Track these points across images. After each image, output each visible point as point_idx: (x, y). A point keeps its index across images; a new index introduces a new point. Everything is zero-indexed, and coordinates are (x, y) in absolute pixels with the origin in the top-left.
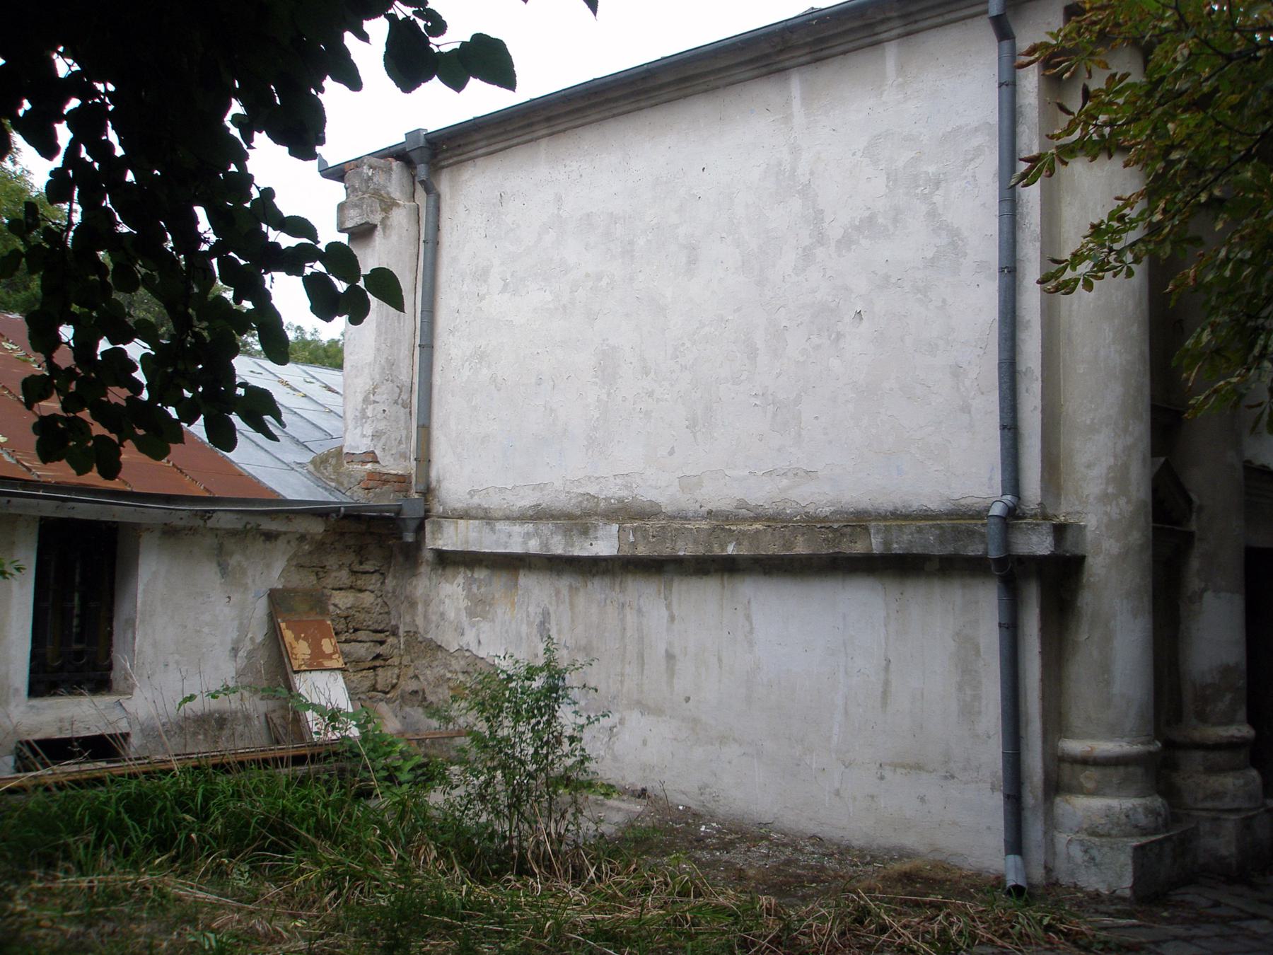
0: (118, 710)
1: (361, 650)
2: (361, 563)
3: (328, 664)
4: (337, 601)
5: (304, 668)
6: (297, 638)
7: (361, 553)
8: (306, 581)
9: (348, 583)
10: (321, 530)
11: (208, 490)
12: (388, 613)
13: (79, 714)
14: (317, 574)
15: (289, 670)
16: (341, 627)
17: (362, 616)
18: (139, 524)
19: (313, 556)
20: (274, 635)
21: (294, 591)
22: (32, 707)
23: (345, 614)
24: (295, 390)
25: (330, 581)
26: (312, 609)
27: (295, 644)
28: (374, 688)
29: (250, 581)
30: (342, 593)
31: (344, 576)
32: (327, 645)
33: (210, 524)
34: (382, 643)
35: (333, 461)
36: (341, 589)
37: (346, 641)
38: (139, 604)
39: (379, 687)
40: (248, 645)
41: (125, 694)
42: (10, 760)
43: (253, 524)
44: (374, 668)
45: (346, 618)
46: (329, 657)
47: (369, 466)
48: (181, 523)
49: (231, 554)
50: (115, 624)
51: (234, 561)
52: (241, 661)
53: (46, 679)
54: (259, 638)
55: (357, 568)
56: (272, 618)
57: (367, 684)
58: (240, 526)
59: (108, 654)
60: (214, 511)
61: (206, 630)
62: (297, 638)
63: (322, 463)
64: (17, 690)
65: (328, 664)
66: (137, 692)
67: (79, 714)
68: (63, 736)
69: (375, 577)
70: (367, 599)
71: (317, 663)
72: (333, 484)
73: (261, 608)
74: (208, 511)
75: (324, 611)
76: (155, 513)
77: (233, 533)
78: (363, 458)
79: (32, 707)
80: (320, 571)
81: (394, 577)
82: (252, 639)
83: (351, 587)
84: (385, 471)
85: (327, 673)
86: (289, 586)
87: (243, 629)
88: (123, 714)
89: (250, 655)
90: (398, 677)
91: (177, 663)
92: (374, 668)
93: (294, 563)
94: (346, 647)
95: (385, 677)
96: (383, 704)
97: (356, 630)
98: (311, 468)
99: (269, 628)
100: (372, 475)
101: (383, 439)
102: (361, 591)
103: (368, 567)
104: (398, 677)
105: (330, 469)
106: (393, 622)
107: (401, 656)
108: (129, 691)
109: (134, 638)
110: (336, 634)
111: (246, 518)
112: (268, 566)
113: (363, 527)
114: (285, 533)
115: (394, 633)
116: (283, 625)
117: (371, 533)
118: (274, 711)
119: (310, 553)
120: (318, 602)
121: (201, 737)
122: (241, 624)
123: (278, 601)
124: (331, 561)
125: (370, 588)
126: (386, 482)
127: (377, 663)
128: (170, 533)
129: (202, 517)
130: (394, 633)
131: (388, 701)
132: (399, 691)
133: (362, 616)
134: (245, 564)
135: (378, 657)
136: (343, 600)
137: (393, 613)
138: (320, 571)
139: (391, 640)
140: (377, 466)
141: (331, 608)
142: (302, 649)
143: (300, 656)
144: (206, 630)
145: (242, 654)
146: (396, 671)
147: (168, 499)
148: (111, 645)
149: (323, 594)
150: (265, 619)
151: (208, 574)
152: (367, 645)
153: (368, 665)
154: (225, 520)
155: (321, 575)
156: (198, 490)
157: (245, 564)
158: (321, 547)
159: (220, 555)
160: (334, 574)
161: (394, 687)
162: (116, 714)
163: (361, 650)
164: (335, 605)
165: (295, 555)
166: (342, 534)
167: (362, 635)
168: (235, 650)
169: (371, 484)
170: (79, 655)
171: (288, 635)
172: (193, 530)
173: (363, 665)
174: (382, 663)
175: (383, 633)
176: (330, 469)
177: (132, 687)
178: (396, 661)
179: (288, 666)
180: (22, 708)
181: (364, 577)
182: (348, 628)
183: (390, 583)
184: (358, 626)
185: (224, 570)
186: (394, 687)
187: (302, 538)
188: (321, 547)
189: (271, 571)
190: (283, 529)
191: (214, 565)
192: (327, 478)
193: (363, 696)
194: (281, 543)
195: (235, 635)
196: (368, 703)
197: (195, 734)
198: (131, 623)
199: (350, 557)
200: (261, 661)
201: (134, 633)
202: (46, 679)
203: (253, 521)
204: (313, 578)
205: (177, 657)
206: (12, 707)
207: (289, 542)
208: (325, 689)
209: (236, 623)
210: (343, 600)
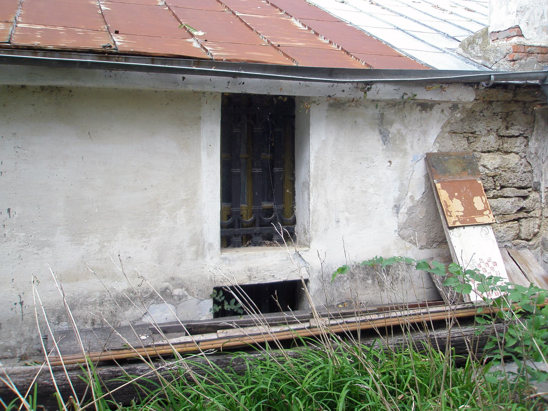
0: (297, 261)
1: (507, 205)
2: (507, 128)
3: (479, 220)
4: (485, 163)
5: (458, 224)
6: (451, 197)
7: (507, 119)
8: (459, 145)
9: (496, 146)
10: (472, 99)
11: (368, 65)
12: (531, 172)
13: (267, 264)
14: (468, 140)
15: (445, 226)
16: (490, 184)
17: (507, 175)
18: (309, 98)
19: (464, 124)
20: (431, 193)
21: (448, 154)
22: (225, 259)
23: (493, 174)
24: (444, 10)
25: (479, 145)
26: (464, 170)
27: (449, 202)
28: (518, 237)
29: (408, 147)
30: (490, 155)
31: (492, 141)
32: (479, 203)
33: (371, 95)
34: (525, 198)
35: (480, 41)
36: (489, 152)
37: (494, 197)
38: (312, 170)
39: (523, 236)
40: (407, 204)
41: (305, 245)
42: (209, 303)
43: (410, 95)
44: (518, 220)
45: (493, 177)
46: (481, 213)
47: (515, 40)
48: (343, 96)
49: (391, 123)
50: (296, 186)
51: (394, 129)
52: (403, 217)
53: (235, 233)
54: (418, 196)
55: (503, 132)
56: (429, 178)
57: (513, 233)
58: (398, 97)
59: (293, 211)
60: (371, 83)
61: (371, 190)
62: (451, 197)
63: (469, 44)
64: (211, 245)
65: (479, 220)
66: (313, 244)
67: (267, 264)
68: (252, 283)
69: (520, 140)
70: (513, 160)
71: (469, 220)
72: (480, 61)
73: (419, 170)
74: (367, 83)
75: (475, 172)
76: (318, 87)
77: (393, 104)
78: (508, 33)
79: (225, 259)
80: (471, 136)
81: (537, 140)
82: (412, 198)
83: (498, 150)
84: (528, 43)
85: (480, 227)
86: (443, 150)
87: (403, 189)
88: (302, 264)
89: (410, 211)
90: (540, 226)
91: (347, 219)
92: (518, 220)
93: (448, 129)
94: (494, 202)
95: (528, 227)
96: (526, 251)
97: (502, 187)
98: (460, 51)
99: (427, 188)
100: (517, 48)
101: (527, 14)
102: (507, 153)
103: (513, 131)
104: (540, 226)
105: (477, 48)
106: (536, 180)
107: (542, 208)
108: (306, 244)
109: (309, 199)
110: (486, 191)
111: (404, 89)
112: (425, 133)
113: (510, 95)
114: (439, 103)
115: (537, 190)
116: (438, 186)
117: (517, 101)
118: (432, 259)
119: (462, 120)
120: (469, 164)
121: (370, 282)
122: (402, 184)
123: (434, 164)
124: (480, 127)
125: (515, 150)
126: (530, 53)
127: (521, 215)
128: (337, 105)
129: (362, 89)
130: (537, 190)
131: (531, 248)
132: (540, 239)
133: (507, 175)
134: (404, 132)
135: (522, 209)
136: (491, 162)
137: (536, 171)
138: (471, 136)
139: (534, 195)
140: (521, 39)
141: (481, 168)
142: (455, 208)
143: (454, 214)
144: (371, 190)
145: (403, 210)
146: (538, 221)
147: (331, 72)
148: (294, 204)
149: (474, 157)
150: (423, 179)
151: (372, 141)
152: (513, 199)
153: (513, 217)
154: (383, 92)
155: (472, 139)
156: (361, 65)
157: (404, 132)
158: (471, 114)
159: (382, 124)
160: (483, 139)
161: (535, 235)
162: (296, 263)
163: (507, 205)
164: (484, 166)
165: (448, 122)
166: (490, 103)
167: (507, 192)
168: (397, 208)
169: (516, 56)
170: (270, 212)
171: (444, 194)
172: (354, 102)
173: (508, 217)
174: (525, 215)
175: (525, 189)
176: (477, 48)
177: (309, 241)
178: (537, 213)
179: (444, 222)
180: (216, 260)
181: (510, 140)
182: (497, 185)
183: (533, 144)
184: (505, 184)
185: (385, 137)
186: (535, 235)
187: (455, 107)
188: (471, 114)
189: (427, 137)
190: (437, 99)
191: (377, 132)
192: (475, 57)
193: (509, 244)
194: (436, 112)
195: (397, 194)
196: (513, 251)
197: (364, 279)
198: (306, 185)
199: (498, 124)
200: (420, 213)
201: (309, 195)
202: (235, 233)
203: (410, 91)
204: (465, 143)
205: (346, 214)
206: (208, 259)
207: (443, 111)
208: (477, 249)
209: (398, 184)
210: (491, 162)
